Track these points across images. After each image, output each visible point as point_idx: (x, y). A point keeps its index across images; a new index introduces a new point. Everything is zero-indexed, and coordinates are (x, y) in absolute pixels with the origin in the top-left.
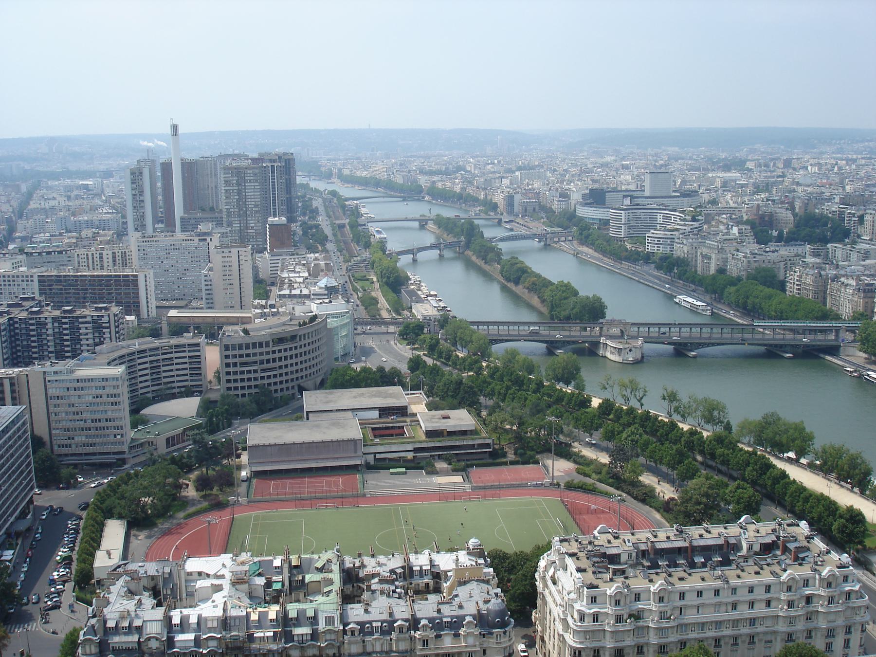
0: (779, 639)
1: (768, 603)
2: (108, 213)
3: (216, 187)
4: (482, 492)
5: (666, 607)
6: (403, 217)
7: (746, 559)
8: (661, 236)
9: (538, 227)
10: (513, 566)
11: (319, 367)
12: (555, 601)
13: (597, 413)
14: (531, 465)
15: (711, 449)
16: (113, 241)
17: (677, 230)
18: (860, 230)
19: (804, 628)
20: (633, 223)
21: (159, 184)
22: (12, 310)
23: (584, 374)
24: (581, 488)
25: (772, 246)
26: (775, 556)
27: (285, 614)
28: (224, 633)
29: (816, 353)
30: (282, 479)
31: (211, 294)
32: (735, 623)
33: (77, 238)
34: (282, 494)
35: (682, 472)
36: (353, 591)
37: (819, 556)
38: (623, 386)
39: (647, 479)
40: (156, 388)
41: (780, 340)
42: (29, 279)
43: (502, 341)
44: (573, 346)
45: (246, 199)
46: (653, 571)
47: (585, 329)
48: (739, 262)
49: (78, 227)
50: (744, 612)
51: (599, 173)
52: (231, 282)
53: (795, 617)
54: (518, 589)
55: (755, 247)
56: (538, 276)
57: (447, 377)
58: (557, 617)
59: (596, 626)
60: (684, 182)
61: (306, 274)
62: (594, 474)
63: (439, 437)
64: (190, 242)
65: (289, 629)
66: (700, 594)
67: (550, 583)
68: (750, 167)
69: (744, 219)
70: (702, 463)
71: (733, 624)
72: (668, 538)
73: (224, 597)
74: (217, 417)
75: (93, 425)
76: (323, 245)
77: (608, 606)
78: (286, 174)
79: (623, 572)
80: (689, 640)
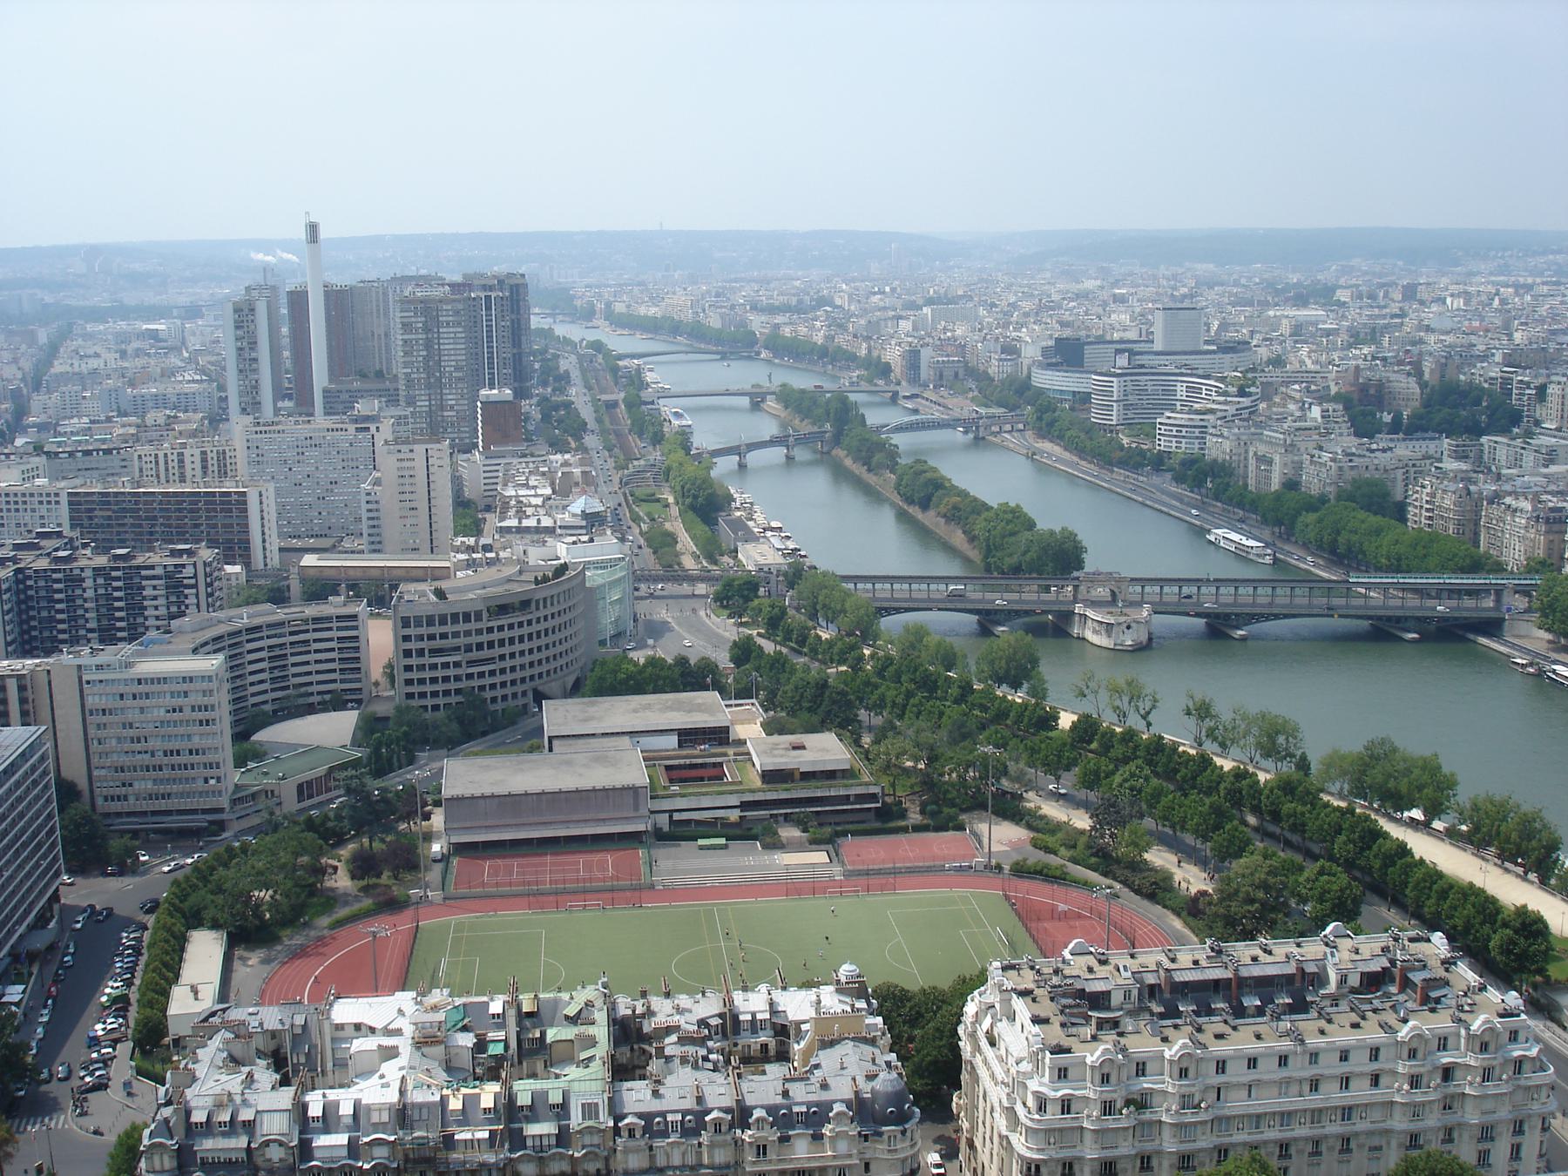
0: (1394, 1143)
1: (1375, 1080)
2: (193, 381)
3: (386, 335)
4: (863, 880)
5: (1191, 1086)
6: (722, 389)
7: (1335, 1000)
8: (1183, 423)
9: (964, 406)
10: (918, 1012)
11: (571, 656)
12: (993, 1076)
13: (1069, 740)
14: (950, 833)
15: (1272, 804)
16: (202, 432)
17: (1212, 411)
18: (1539, 412)
19: (1439, 1124)
20: (1132, 399)
21: (285, 330)
22: (21, 554)
23: (1046, 669)
24: (1040, 873)
25: (1382, 440)
26: (1388, 995)
27: (511, 1098)
28: (401, 1133)
29: (1461, 633)
30: (504, 857)
31: (378, 526)
32: (1316, 1115)
33: (138, 426)
34: (504, 885)
35: (1221, 845)
36: (632, 1057)
37: (1466, 995)
38: (1116, 691)
39: (1159, 857)
40: (280, 694)
41: (1397, 608)
42: (53, 499)
43: (898, 610)
44: (1026, 619)
45: (440, 355)
46: (1168, 1022)
47: (1047, 589)
48: (1324, 470)
49: (139, 407)
50: (1332, 1095)
51: (1073, 310)
52: (413, 505)
53: (1423, 1104)
54: (928, 1054)
55: (1352, 443)
56: (964, 494)
57: (799, 675)
58: (997, 1105)
59: (1067, 1121)
60: (1224, 326)
61: (548, 491)
62: (1062, 849)
63: (786, 782)
64: (339, 433)
65: (516, 1125)
66: (1252, 1062)
67: (984, 1043)
68: (1343, 299)
69: (1333, 393)
70: (1256, 829)
71: (1313, 1116)
72: (1196, 962)
73: (401, 1069)
74: (388, 746)
75: (166, 760)
76: (578, 438)
77: (1089, 1085)
78: (512, 312)
79: (1115, 1024)
80: (1234, 1145)
